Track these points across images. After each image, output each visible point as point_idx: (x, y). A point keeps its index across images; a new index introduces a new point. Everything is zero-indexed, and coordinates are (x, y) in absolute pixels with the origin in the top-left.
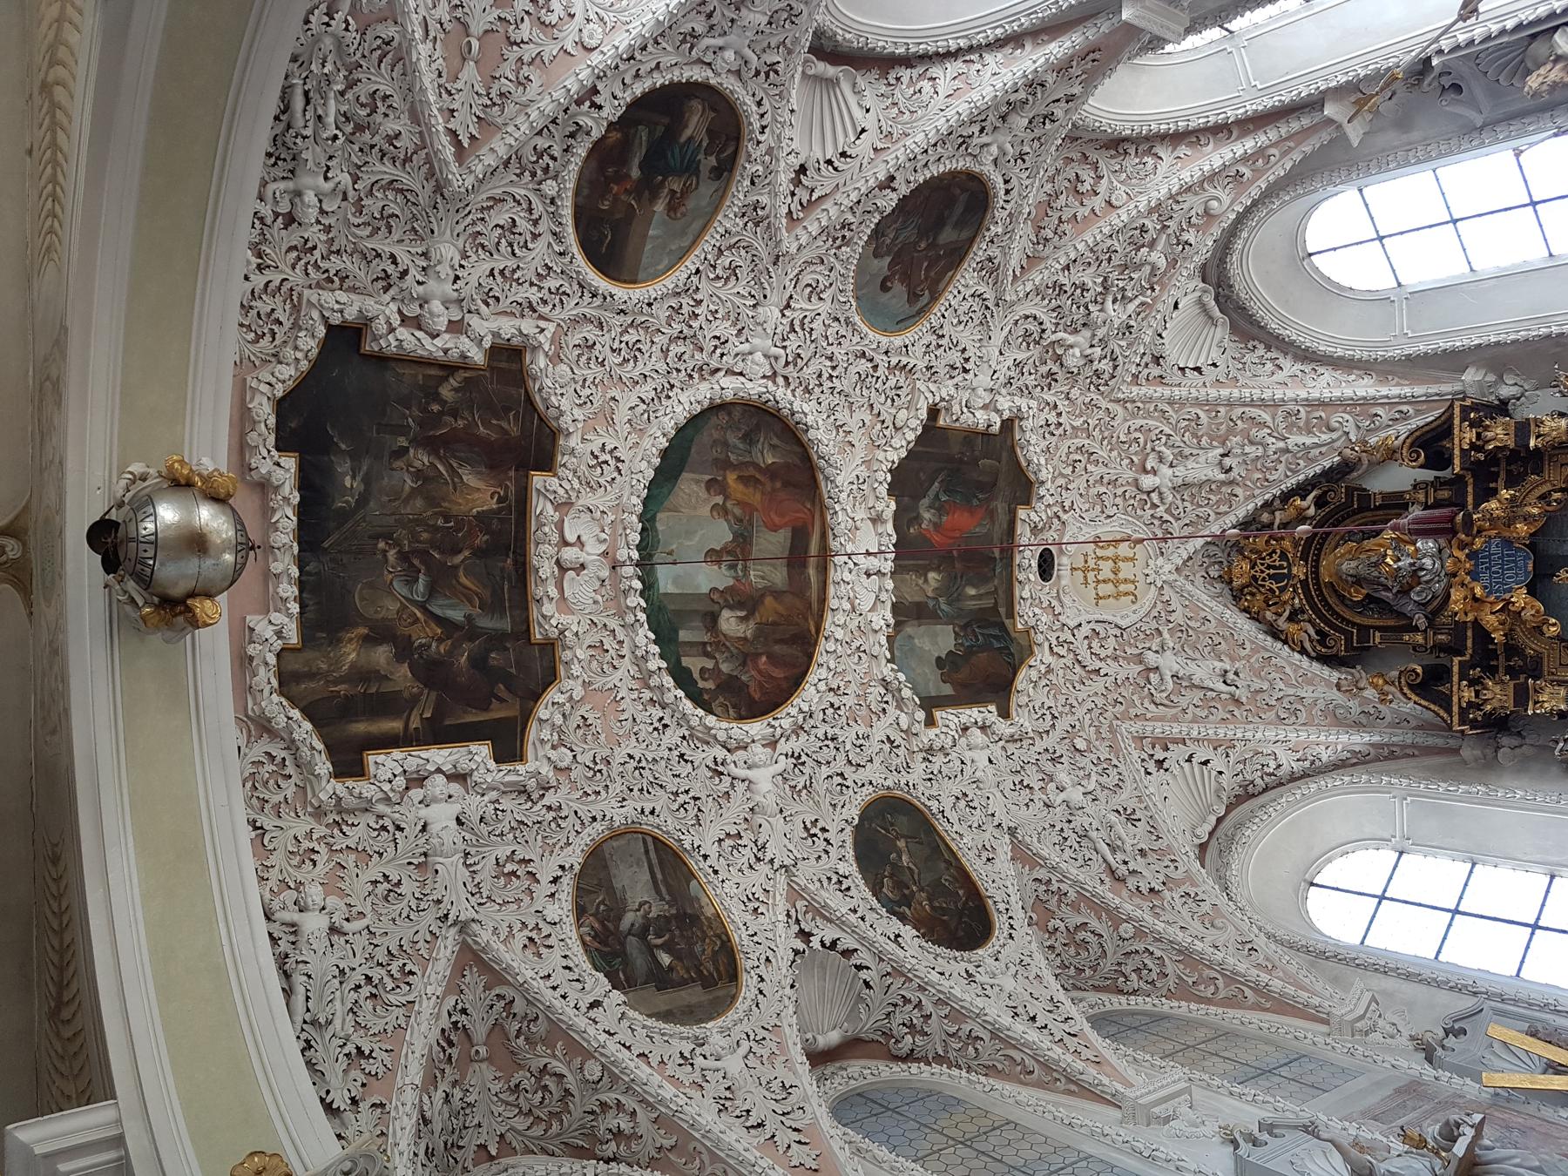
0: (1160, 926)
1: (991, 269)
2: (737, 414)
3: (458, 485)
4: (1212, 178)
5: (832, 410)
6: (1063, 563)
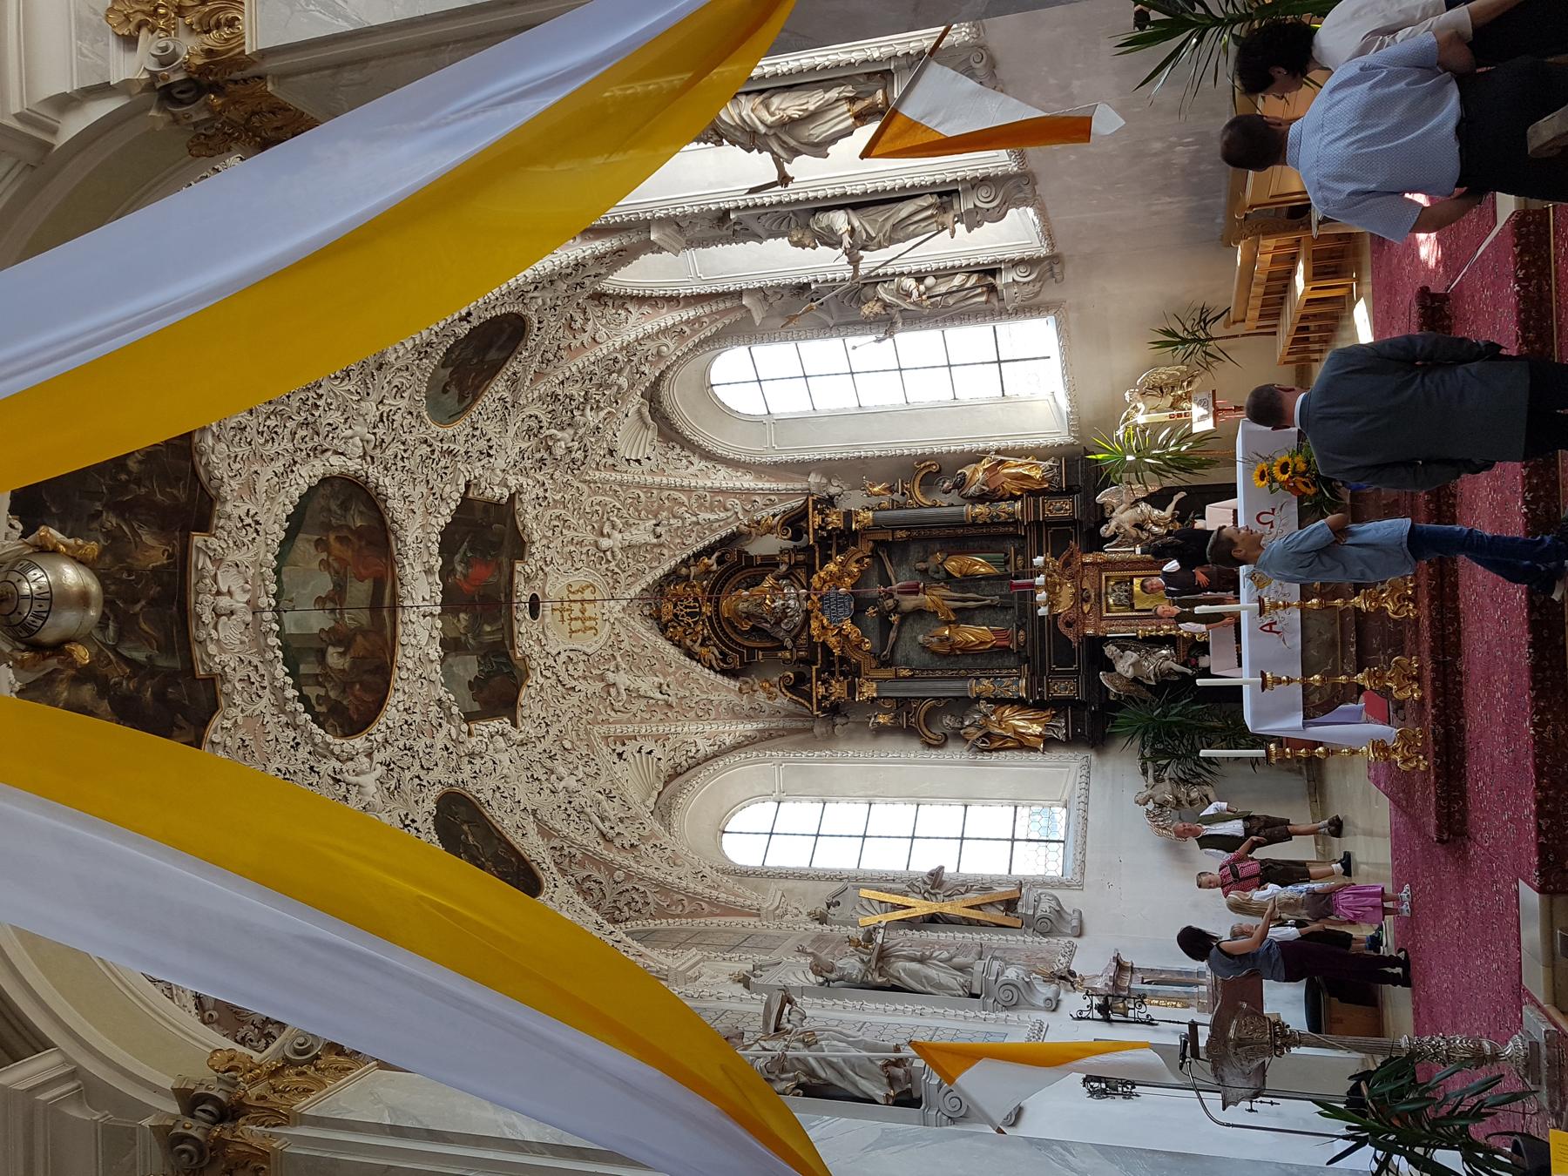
0: (642, 870)
1: (514, 381)
2: (337, 484)
3: (139, 544)
4: (664, 331)
5: (401, 485)
6: (546, 609)
